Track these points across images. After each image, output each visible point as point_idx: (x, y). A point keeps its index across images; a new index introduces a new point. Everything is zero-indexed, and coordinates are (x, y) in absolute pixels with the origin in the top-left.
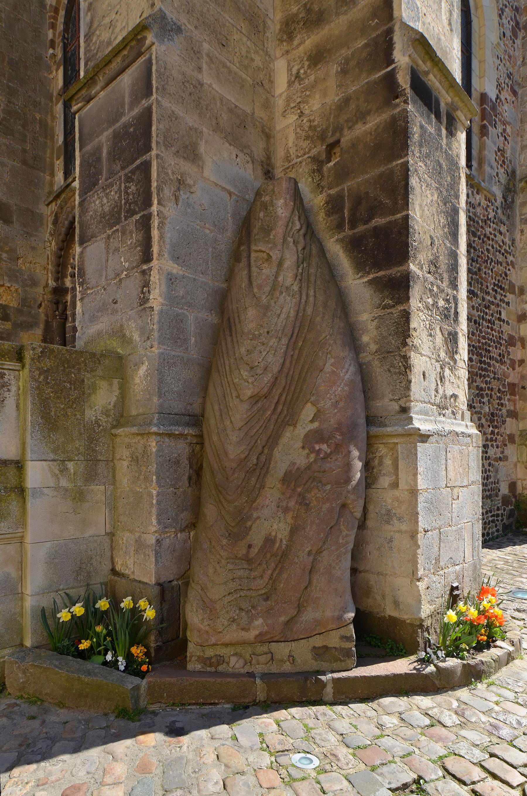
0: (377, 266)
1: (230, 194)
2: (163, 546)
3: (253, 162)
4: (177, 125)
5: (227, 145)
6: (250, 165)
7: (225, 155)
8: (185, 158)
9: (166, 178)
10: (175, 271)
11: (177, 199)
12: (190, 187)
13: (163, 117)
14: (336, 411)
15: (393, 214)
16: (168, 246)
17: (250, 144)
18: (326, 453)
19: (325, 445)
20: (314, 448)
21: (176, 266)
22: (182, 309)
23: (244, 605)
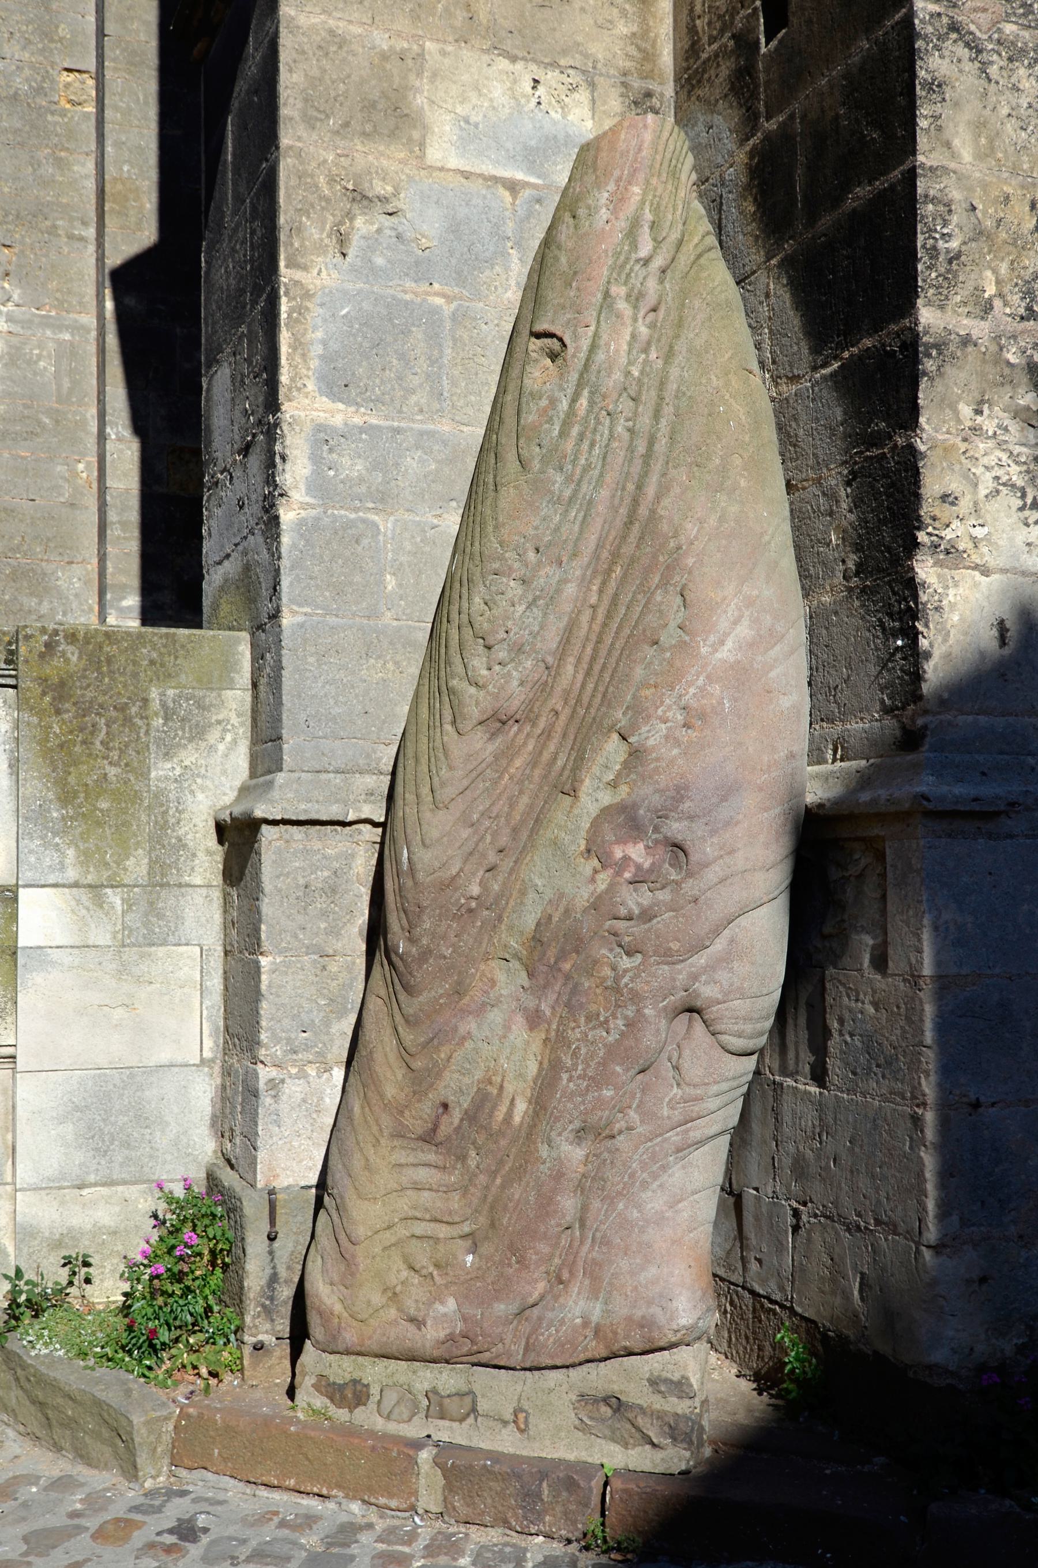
1: (513, 187)
2: (284, 1098)
3: (592, 85)
4: (344, 60)
5: (503, 64)
6: (583, 96)
7: (498, 91)
8: (364, 134)
9: (312, 198)
10: (338, 421)
11: (342, 241)
12: (383, 200)
13: (303, 52)
14: (675, 752)
16: (314, 364)
17: (579, 39)
18: (639, 867)
20: (610, 854)
21: (341, 406)
22: (356, 510)
23: (423, 1260)
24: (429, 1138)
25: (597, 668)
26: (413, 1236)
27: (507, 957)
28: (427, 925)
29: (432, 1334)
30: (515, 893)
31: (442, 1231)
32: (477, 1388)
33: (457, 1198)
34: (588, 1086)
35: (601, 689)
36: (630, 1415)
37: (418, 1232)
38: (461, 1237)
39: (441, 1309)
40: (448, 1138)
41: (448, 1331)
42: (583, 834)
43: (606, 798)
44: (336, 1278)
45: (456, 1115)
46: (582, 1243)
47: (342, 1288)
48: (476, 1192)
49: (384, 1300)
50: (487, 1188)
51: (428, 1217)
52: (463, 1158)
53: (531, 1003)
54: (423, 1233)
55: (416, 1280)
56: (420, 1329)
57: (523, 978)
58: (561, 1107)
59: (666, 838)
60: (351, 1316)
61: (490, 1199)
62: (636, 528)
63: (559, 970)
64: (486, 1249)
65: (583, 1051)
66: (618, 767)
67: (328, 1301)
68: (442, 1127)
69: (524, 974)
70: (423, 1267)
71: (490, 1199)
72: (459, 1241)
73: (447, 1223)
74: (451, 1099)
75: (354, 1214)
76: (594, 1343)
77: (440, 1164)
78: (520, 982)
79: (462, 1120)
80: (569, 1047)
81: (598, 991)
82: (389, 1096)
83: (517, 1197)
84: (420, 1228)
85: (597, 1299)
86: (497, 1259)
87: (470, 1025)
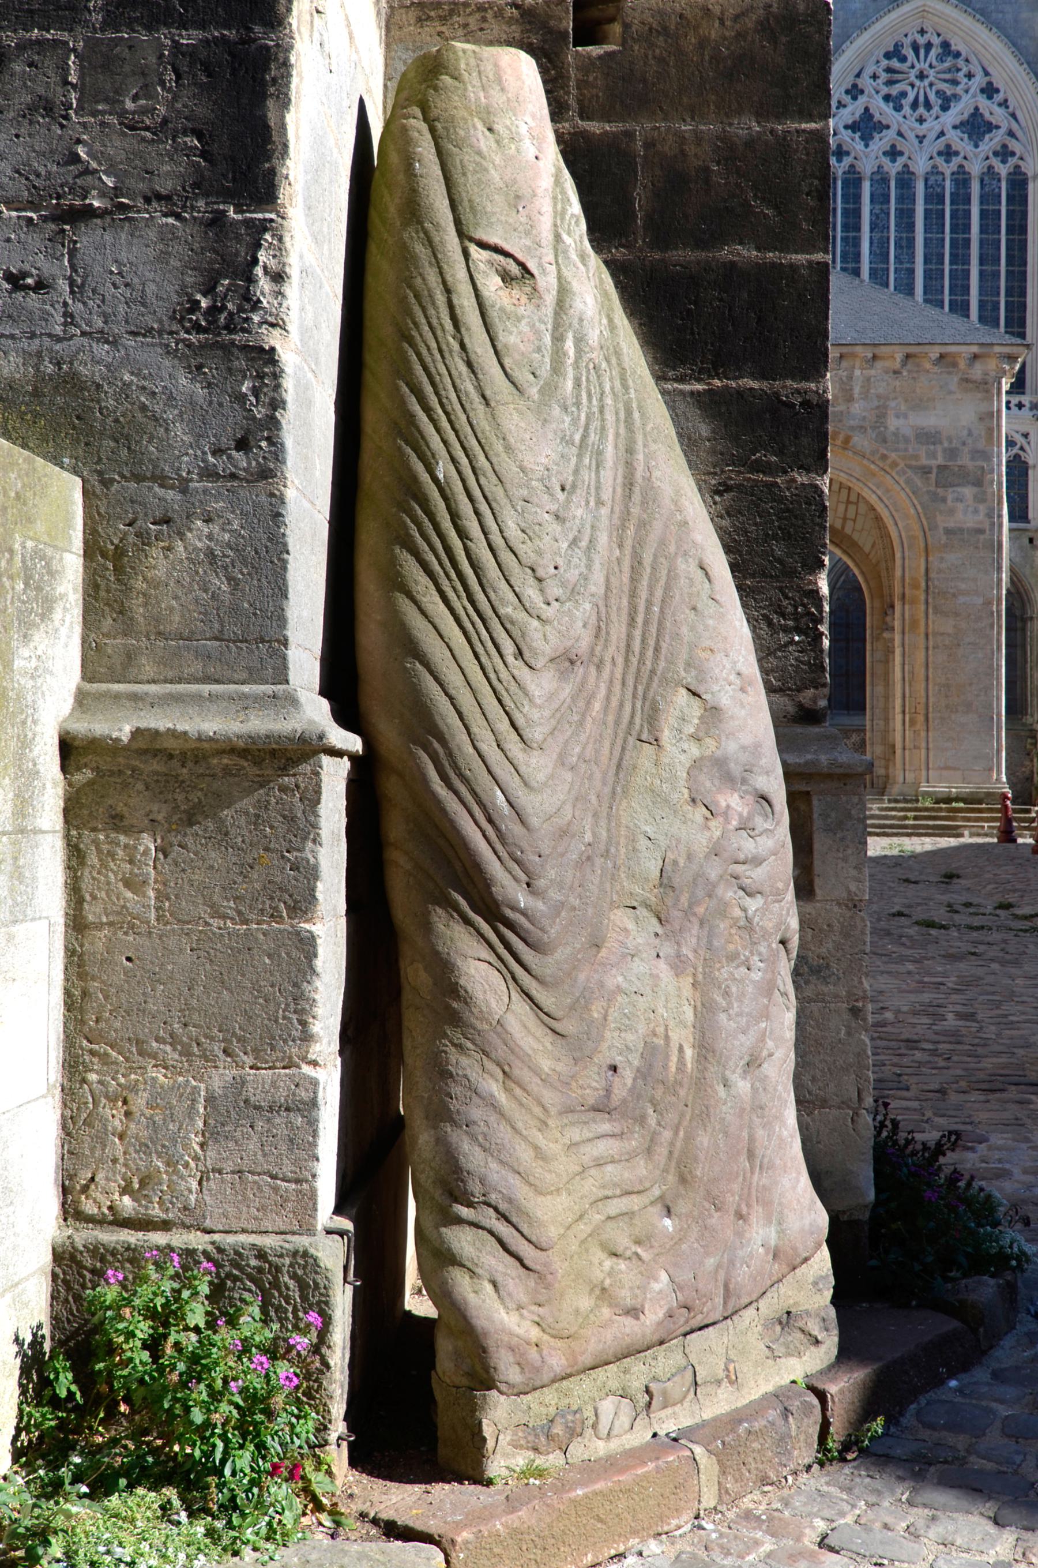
0: (719, 365)
15: (785, 249)
19: (736, 796)
23: (623, 1241)
24: (602, 1108)
25: (640, 619)
26: (609, 1218)
27: (635, 904)
28: (552, 874)
29: (653, 1316)
30: (622, 841)
31: (634, 1202)
32: (694, 1360)
33: (642, 1162)
34: (748, 1022)
35: (652, 642)
36: (800, 1324)
37: (613, 1212)
38: (652, 1203)
39: (656, 1286)
40: (624, 1101)
41: (665, 1308)
42: (683, 783)
43: (695, 751)
44: (524, 1298)
45: (628, 1075)
46: (752, 1173)
47: (535, 1308)
48: (662, 1151)
49: (592, 1302)
50: (672, 1144)
51: (618, 1192)
52: (642, 1120)
53: (667, 949)
54: (618, 1211)
55: (622, 1265)
56: (637, 1318)
57: (654, 925)
58: (729, 1046)
59: (756, 790)
60: (554, 1337)
61: (676, 1154)
62: (637, 497)
63: (695, 914)
64: (682, 1207)
65: (734, 989)
66: (696, 721)
67: (520, 1331)
68: (616, 1091)
69: (654, 921)
70: (626, 1248)
71: (676, 1154)
72: (650, 1209)
73: (638, 1192)
74: (619, 1060)
75: (539, 1214)
76: (776, 1266)
77: (617, 1131)
78: (652, 930)
79: (635, 1080)
80: (720, 988)
81: (733, 931)
82: (546, 1069)
83: (706, 1144)
84: (615, 1207)
85: (771, 1223)
86: (695, 1213)
87: (615, 979)
